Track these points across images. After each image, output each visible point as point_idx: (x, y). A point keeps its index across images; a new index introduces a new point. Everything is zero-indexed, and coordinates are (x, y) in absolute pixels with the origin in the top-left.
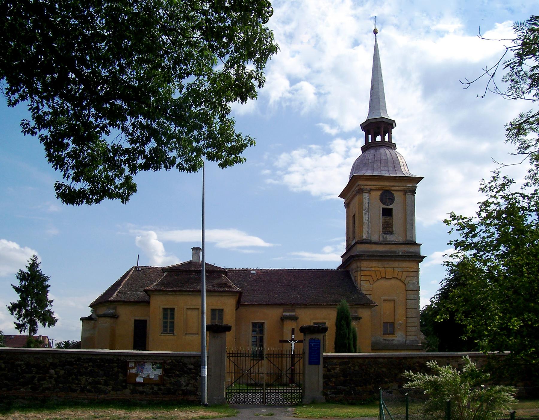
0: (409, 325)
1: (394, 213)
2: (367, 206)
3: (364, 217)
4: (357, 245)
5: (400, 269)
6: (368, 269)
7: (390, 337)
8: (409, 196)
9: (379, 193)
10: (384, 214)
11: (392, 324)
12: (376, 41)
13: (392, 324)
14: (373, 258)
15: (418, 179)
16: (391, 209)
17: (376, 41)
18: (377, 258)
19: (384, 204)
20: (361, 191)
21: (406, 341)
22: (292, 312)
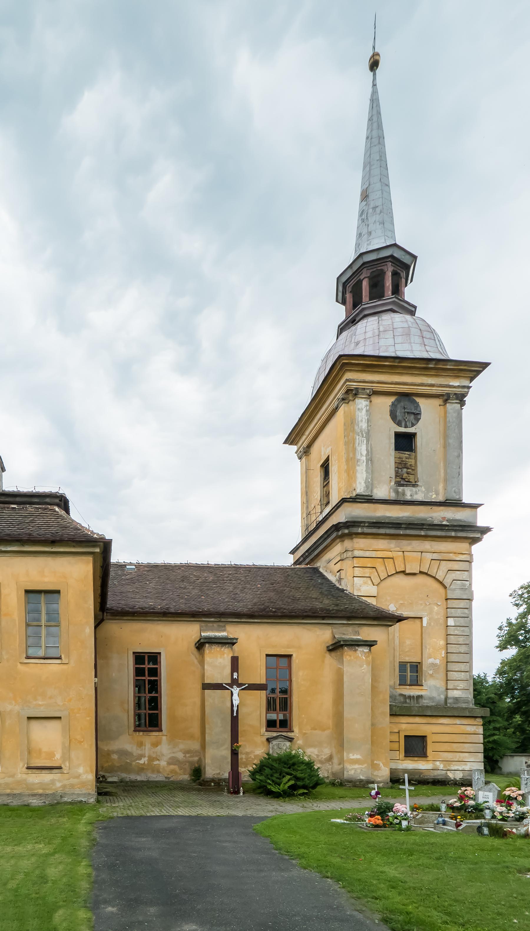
0: (451, 667)
1: (419, 441)
2: (364, 425)
3: (358, 448)
4: (346, 504)
5: (435, 556)
6: (367, 554)
7: (413, 691)
8: (452, 406)
9: (390, 400)
10: (398, 447)
11: (416, 667)
12: (374, 85)
13: (416, 667)
14: (382, 531)
15: (473, 369)
16: (414, 435)
17: (374, 85)
18: (388, 531)
19: (399, 424)
20: (352, 394)
21: (446, 698)
22: (219, 631)
